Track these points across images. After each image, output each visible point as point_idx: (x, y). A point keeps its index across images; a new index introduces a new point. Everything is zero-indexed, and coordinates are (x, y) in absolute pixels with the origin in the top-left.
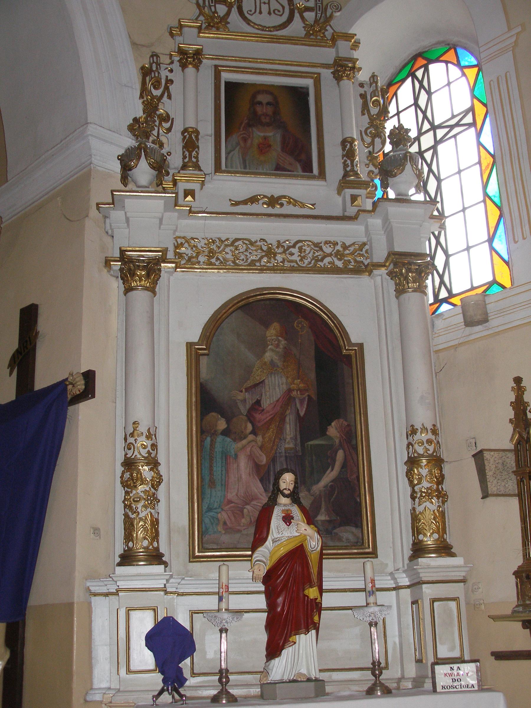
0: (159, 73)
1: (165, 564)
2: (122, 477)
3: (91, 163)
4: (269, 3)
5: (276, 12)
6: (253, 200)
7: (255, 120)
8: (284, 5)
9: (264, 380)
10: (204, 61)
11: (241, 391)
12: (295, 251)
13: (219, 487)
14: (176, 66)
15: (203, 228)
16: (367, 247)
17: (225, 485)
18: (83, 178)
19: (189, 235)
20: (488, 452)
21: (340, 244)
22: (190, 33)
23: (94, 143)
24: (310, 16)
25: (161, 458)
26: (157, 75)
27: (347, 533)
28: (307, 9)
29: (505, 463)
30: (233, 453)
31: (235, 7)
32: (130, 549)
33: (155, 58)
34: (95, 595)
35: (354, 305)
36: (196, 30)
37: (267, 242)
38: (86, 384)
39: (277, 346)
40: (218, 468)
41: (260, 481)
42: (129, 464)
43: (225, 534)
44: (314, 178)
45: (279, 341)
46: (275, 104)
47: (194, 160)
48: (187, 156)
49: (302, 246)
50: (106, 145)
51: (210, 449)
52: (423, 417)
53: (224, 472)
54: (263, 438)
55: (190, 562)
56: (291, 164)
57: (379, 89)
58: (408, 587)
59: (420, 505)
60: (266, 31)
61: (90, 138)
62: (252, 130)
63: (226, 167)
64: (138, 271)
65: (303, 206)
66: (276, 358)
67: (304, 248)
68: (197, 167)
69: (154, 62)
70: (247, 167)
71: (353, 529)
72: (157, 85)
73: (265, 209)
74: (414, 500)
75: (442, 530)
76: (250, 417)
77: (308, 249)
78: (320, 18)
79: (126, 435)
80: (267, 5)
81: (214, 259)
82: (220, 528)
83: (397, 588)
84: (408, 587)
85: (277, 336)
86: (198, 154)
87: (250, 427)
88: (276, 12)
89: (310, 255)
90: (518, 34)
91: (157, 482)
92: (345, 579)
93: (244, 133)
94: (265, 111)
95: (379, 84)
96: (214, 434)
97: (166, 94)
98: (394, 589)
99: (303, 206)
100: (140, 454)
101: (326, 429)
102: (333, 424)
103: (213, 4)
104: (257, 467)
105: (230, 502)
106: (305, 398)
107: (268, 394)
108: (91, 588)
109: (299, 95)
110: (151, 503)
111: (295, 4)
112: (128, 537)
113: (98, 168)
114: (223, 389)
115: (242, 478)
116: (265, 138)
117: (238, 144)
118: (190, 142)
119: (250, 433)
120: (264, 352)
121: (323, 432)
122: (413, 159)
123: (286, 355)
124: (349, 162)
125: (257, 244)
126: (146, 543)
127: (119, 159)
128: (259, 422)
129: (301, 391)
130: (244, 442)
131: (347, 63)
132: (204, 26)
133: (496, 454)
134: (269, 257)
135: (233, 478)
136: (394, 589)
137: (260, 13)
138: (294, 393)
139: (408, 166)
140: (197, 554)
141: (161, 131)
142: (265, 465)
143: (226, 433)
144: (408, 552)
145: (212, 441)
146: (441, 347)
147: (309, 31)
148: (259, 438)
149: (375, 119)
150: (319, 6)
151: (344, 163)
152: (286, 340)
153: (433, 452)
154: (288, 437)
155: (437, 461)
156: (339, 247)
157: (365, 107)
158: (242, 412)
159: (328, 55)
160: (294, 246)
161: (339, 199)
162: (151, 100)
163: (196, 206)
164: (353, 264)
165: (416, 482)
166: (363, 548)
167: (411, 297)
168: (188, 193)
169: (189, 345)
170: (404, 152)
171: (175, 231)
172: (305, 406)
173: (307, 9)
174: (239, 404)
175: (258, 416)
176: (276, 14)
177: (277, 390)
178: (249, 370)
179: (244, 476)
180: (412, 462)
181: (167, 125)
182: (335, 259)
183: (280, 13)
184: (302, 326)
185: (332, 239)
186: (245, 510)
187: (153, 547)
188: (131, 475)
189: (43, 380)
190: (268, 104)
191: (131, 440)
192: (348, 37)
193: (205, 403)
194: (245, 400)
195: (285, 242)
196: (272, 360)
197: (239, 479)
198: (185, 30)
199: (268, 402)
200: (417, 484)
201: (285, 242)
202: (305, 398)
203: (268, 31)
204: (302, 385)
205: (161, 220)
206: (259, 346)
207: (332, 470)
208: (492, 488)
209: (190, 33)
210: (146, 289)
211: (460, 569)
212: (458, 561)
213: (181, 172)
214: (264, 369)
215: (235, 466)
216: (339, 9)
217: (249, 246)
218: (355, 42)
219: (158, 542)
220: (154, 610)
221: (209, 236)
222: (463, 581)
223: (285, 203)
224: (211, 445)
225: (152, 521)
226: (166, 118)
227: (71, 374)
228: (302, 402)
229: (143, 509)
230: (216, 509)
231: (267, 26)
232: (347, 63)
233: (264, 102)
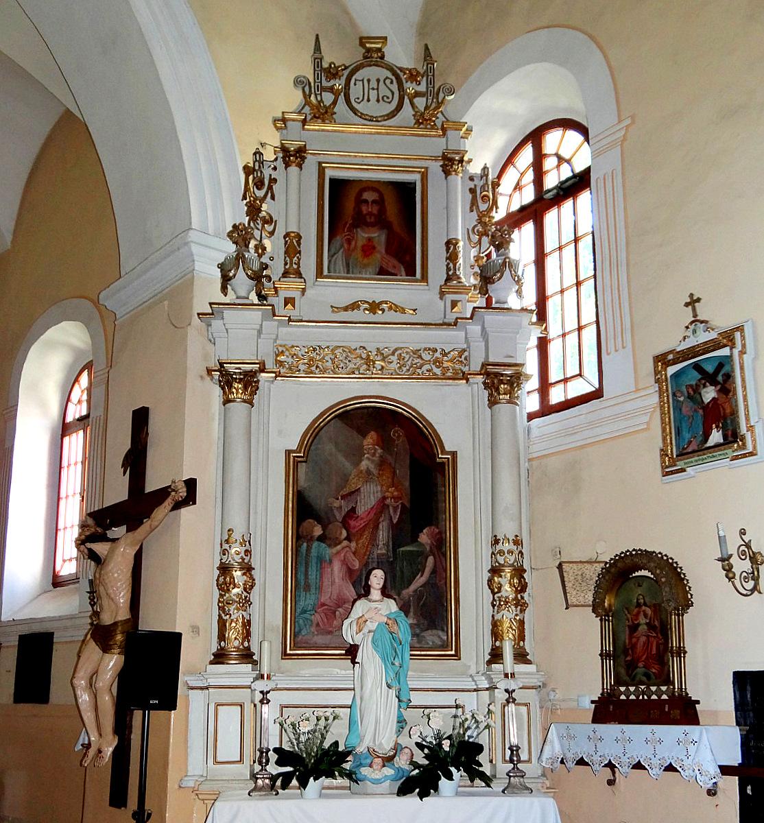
0: (261, 172)
1: (255, 663)
2: (218, 580)
3: (194, 270)
4: (378, 89)
5: (385, 98)
6: (354, 306)
7: (360, 221)
8: (393, 90)
9: (359, 488)
10: (309, 157)
11: (338, 499)
12: (394, 358)
13: (313, 591)
14: (280, 164)
15: (301, 336)
16: (466, 354)
17: (320, 589)
18: (185, 284)
19: (290, 343)
20: (567, 564)
21: (439, 351)
22: (295, 127)
23: (195, 249)
24: (420, 102)
25: (255, 562)
26: (259, 175)
27: (431, 637)
28: (417, 94)
29: (584, 575)
30: (328, 559)
31: (342, 94)
32: (222, 649)
33: (258, 155)
34: (192, 688)
35: (450, 413)
36: (300, 124)
37: (366, 350)
38: (188, 492)
39: (374, 455)
41: (353, 585)
42: (225, 569)
43: (317, 635)
44: (416, 281)
45: (376, 450)
46: (380, 202)
47: (295, 266)
48: (288, 262)
49: (400, 354)
50: (209, 251)
51: (306, 554)
52: (507, 529)
53: (318, 577)
54: (357, 545)
55: (282, 659)
56: (395, 267)
57: (490, 183)
58: (487, 689)
59: (498, 612)
60: (372, 121)
61: (192, 245)
62: (357, 231)
64: (239, 382)
65: (403, 311)
66: (372, 467)
67: (403, 355)
68: (300, 275)
69: (256, 160)
70: (350, 270)
71: (440, 633)
72: (259, 184)
73: (368, 316)
74: (494, 608)
76: (345, 523)
77: (407, 357)
78: (431, 104)
79: (221, 541)
80: (376, 91)
81: (315, 367)
82: (313, 629)
84: (487, 689)
85: (373, 445)
86: (299, 260)
87: (344, 533)
88: (385, 98)
89: (409, 363)
90: (627, 127)
91: (248, 588)
92: (428, 679)
93: (348, 235)
94: (370, 210)
95: (490, 177)
96: (310, 539)
97: (270, 194)
98: (475, 690)
99: (403, 311)
100: (234, 560)
101: (418, 537)
102: (424, 531)
103: (319, 92)
104: (350, 572)
105: (323, 605)
106: (398, 506)
107: (363, 501)
108: (188, 682)
109: (405, 193)
110: (243, 606)
111: (405, 88)
112: (222, 637)
113: (202, 274)
114: (320, 497)
115: (336, 580)
116: (370, 239)
117: (342, 246)
118: (292, 247)
119: (345, 539)
120: (361, 461)
121: (414, 539)
122: (512, 266)
123: (382, 464)
124: (451, 265)
125: (358, 351)
126: (236, 643)
127: (219, 268)
128: (354, 528)
129: (396, 498)
130: (339, 547)
131: (453, 156)
132: (309, 118)
133: (575, 566)
134: (367, 363)
135: (326, 582)
136: (475, 690)
137: (368, 100)
138: (388, 501)
139: (507, 272)
140: (288, 652)
141: (263, 235)
142: (357, 570)
143: (322, 539)
144: (488, 657)
145: (308, 546)
146: (535, 455)
147: (419, 120)
148: (353, 545)
149: (484, 216)
150: (431, 90)
151: (447, 266)
152: (382, 448)
153: (514, 563)
155: (519, 572)
156: (438, 355)
157: (474, 203)
158: (338, 518)
159: (436, 145)
160: (393, 354)
161: (442, 303)
162: (254, 201)
163: (295, 314)
164: (451, 371)
165: (496, 590)
166: (450, 648)
167: (503, 409)
168: (289, 301)
169: (287, 452)
170: (504, 257)
171: (275, 341)
172: (398, 514)
173: (417, 94)
174: (335, 511)
175: (352, 523)
176: (386, 102)
177: (372, 498)
178: (346, 479)
179: (337, 580)
180: (495, 571)
181: (269, 228)
182: (433, 367)
183: (389, 100)
184: (396, 433)
185: (431, 346)
186: (337, 613)
187: (244, 647)
188: (225, 579)
189: (152, 485)
190: (374, 202)
191: (226, 546)
192: (458, 125)
193: (303, 510)
194: (341, 507)
195: (383, 349)
196: (368, 468)
197: (333, 583)
198: (289, 124)
199: (363, 510)
200: (497, 593)
201: (383, 349)
202: (398, 506)
203: (375, 121)
204: (396, 493)
205: (260, 332)
206: (356, 454)
207: (422, 576)
208: (572, 600)
209: (295, 127)
210: (244, 401)
211: (533, 676)
213: (282, 279)
214: (359, 477)
215: (329, 570)
216: (451, 92)
217: (349, 354)
218: (467, 130)
219: (249, 641)
220: (241, 705)
221: (310, 344)
222: (192, 688)
223: (386, 309)
224: (307, 551)
225: (243, 623)
226: (269, 220)
227: (174, 482)
228: (395, 509)
229: (236, 611)
230: (310, 611)
231: (375, 116)
232: (453, 156)
233: (370, 200)
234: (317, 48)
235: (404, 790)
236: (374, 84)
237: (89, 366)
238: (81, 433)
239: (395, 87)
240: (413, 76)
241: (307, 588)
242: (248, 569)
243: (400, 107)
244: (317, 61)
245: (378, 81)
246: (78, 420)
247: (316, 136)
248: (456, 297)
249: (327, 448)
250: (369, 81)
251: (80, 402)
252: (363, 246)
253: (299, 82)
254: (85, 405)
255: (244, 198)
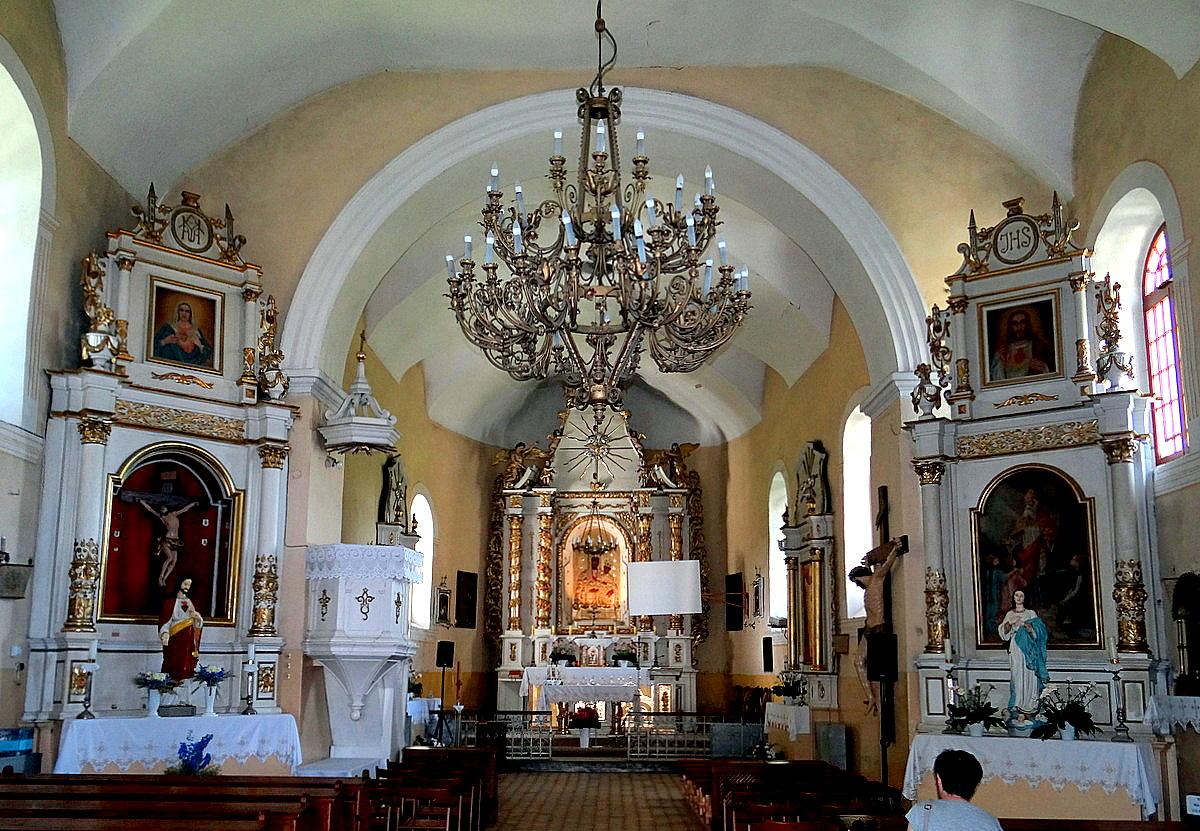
7: (1013, 338)
13: (996, 603)
28: (1048, 234)
34: (33, 650)
35: (1083, 468)
40: (994, 590)
46: (1027, 321)
63: (991, 379)
66: (1030, 513)
75: (1142, 631)
83: (46, 650)
87: (1015, 563)
90: (1190, 245)
91: (945, 605)
123: (1038, 512)
148: (1022, 570)
154: (1042, 568)
155: (273, 578)
173: (1048, 234)
190: (1022, 321)
193: (989, 549)
212: (279, 640)
222: (33, 650)
234: (972, 220)
235: (1034, 735)
236: (1015, 235)
237: (1163, 227)
238: (1166, 301)
239: (1031, 233)
240: (1045, 219)
241: (992, 601)
242: (944, 592)
243: (1036, 246)
244: (972, 227)
245: (1018, 232)
246: (1161, 287)
247: (976, 288)
248: (1083, 384)
249: (999, 502)
250: (1011, 234)
251: (1159, 268)
252: (1015, 356)
253: (962, 248)
254: (1165, 270)
255: (929, 341)
